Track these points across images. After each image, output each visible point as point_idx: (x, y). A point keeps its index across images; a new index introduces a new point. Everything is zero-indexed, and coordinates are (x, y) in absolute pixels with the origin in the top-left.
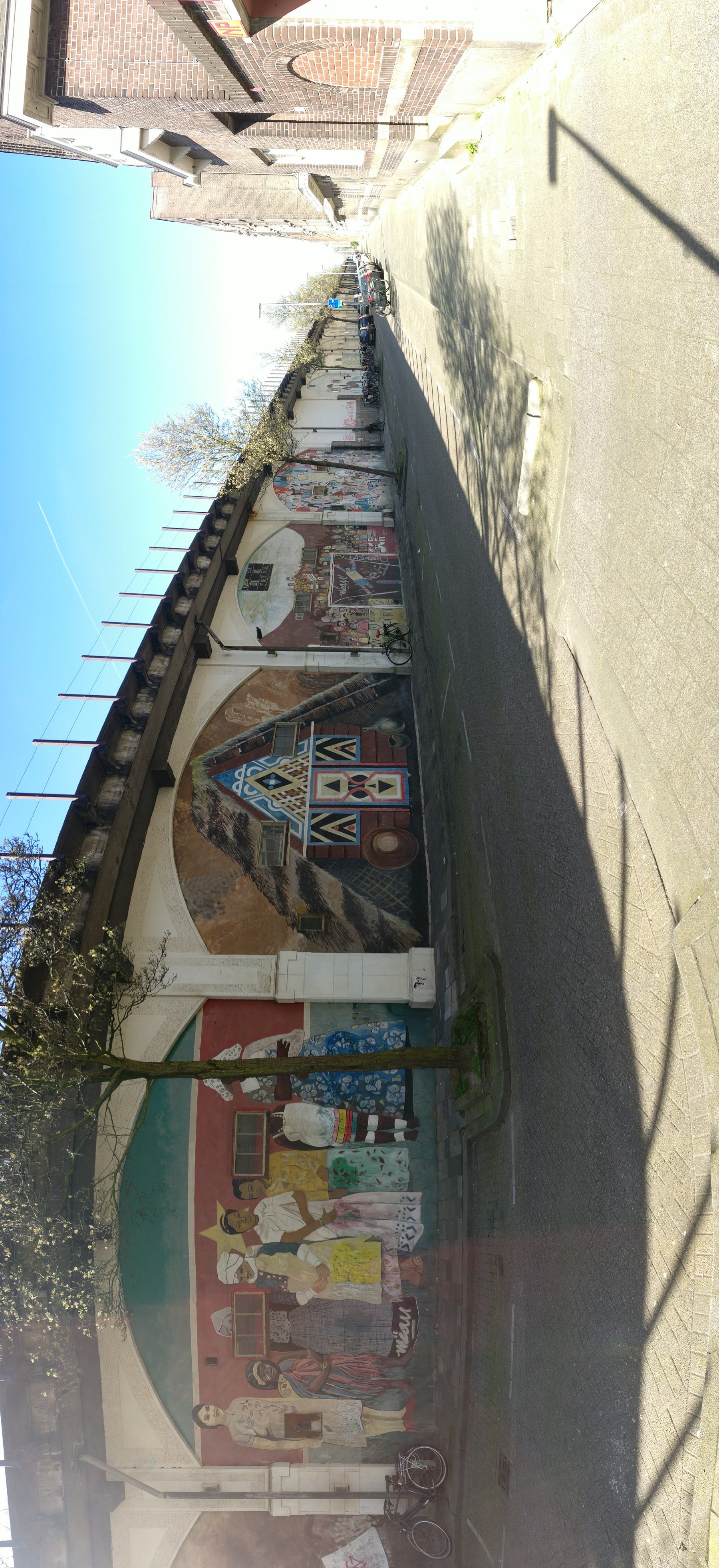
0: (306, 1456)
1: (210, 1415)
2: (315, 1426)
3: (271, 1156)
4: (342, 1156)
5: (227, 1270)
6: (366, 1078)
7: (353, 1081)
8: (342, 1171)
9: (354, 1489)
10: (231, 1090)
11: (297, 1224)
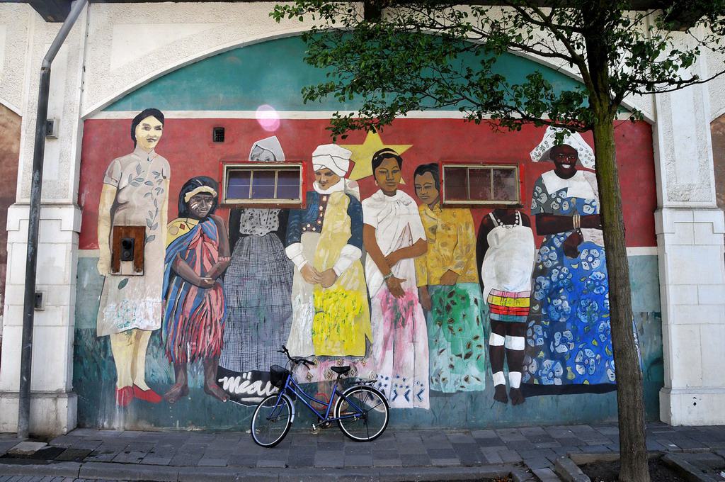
0: (87, 253)
1: (149, 130)
2: (127, 267)
3: (467, 211)
4: (472, 302)
5: (328, 156)
6: (569, 332)
7: (565, 315)
8: (453, 303)
9: (37, 317)
10: (544, 159)
11: (386, 245)
